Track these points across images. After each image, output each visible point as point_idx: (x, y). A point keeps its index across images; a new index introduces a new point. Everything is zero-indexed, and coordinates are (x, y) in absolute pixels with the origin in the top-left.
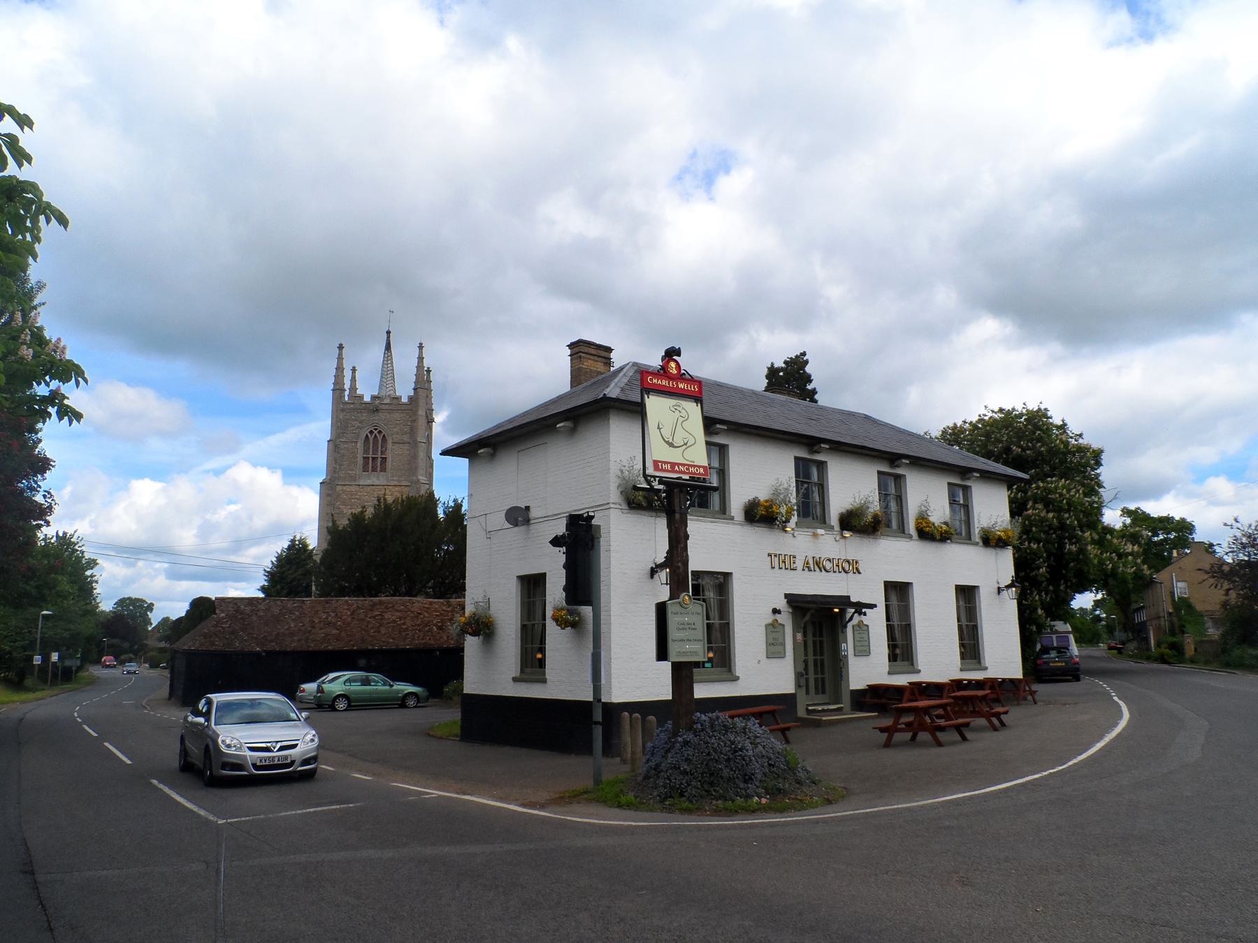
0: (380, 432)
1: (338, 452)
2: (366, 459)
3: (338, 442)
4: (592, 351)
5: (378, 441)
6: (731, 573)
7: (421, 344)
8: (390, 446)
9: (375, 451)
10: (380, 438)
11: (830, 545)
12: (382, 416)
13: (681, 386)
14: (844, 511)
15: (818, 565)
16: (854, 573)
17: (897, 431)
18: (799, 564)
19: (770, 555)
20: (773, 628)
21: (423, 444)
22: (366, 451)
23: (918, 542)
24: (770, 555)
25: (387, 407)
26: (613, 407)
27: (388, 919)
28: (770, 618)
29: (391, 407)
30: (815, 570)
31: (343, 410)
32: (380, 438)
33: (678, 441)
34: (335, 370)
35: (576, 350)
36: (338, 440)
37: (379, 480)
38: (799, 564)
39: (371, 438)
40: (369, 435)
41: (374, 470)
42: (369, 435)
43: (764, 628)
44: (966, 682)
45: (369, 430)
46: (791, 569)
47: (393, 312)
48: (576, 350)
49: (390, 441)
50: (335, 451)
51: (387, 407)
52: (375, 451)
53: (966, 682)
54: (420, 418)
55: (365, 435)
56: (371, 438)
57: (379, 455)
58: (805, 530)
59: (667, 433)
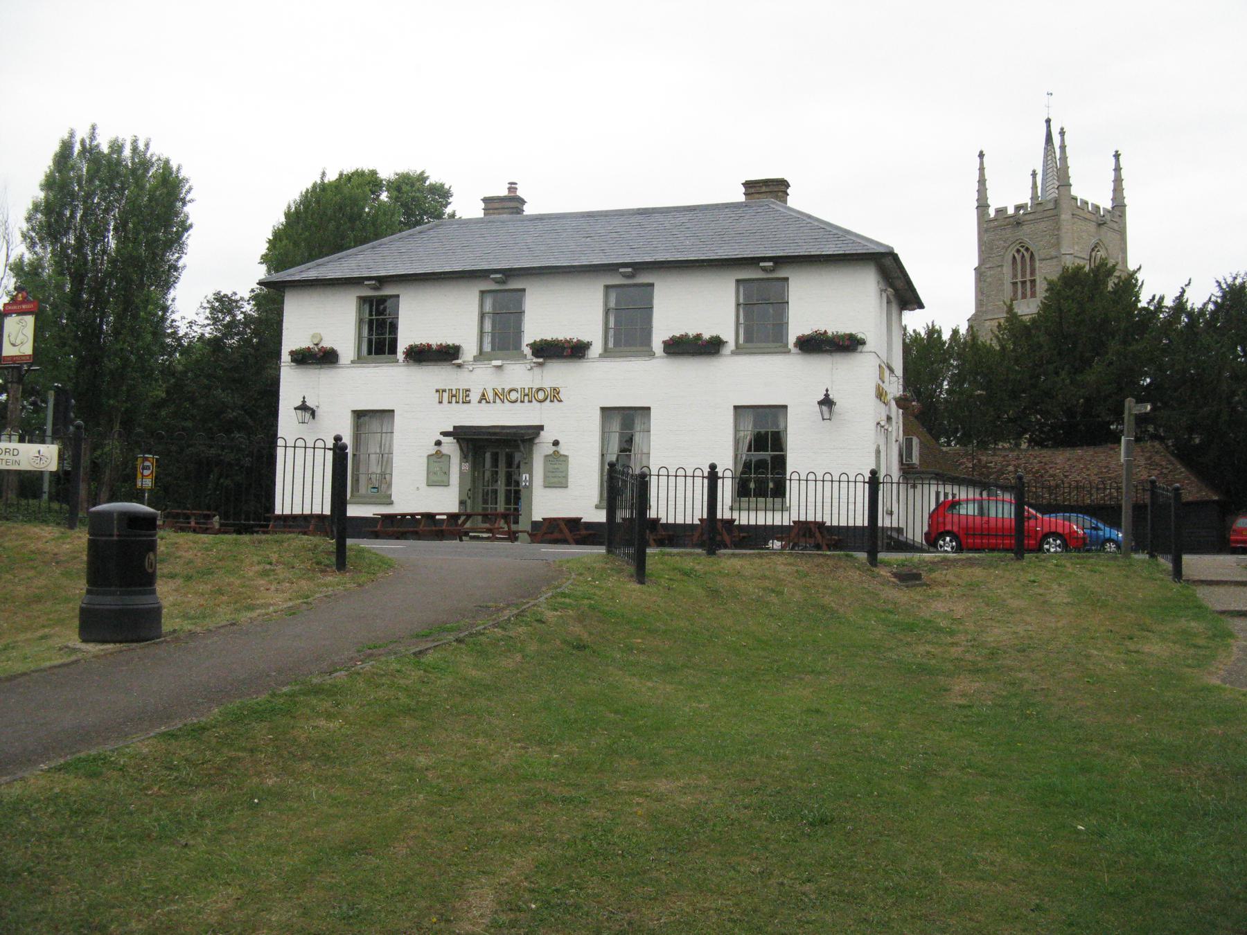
0: (1027, 249)
1: (984, 281)
2: (1015, 284)
3: (983, 270)
4: (497, 205)
5: (1025, 260)
6: (785, 407)
7: (1062, 129)
8: (1037, 264)
9: (1023, 275)
10: (1027, 255)
11: (520, 374)
12: (1026, 228)
13: (24, 307)
14: (444, 344)
15: (501, 396)
16: (551, 401)
17: (583, 217)
18: (475, 397)
19: (437, 391)
20: (437, 458)
21: (1068, 256)
22: (1015, 276)
23: (665, 360)
24: (437, 391)
25: (1031, 217)
26: (287, 286)
27: (56, 550)
28: (433, 449)
29: (1037, 216)
30: (494, 402)
31: (986, 231)
32: (1027, 255)
33: (18, 342)
34: (1113, 172)
35: (490, 206)
36: (983, 267)
37: (1029, 307)
38: (475, 397)
39: (1018, 257)
40: (1016, 255)
41: (1024, 296)
42: (1016, 255)
43: (426, 460)
44: (419, 517)
45: (1015, 249)
46: (463, 402)
47: (1051, 94)
48: (490, 206)
49: (1037, 257)
50: (980, 281)
51: (1031, 217)
52: (1023, 275)
53: (419, 517)
54: (1065, 223)
55: (1011, 255)
56: (1018, 257)
57: (1028, 277)
58: (486, 362)
59: (12, 340)
